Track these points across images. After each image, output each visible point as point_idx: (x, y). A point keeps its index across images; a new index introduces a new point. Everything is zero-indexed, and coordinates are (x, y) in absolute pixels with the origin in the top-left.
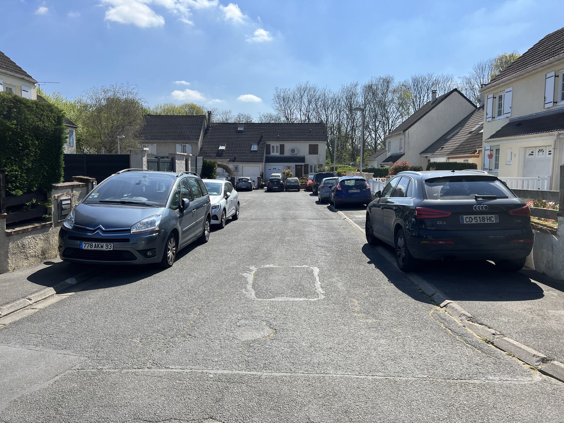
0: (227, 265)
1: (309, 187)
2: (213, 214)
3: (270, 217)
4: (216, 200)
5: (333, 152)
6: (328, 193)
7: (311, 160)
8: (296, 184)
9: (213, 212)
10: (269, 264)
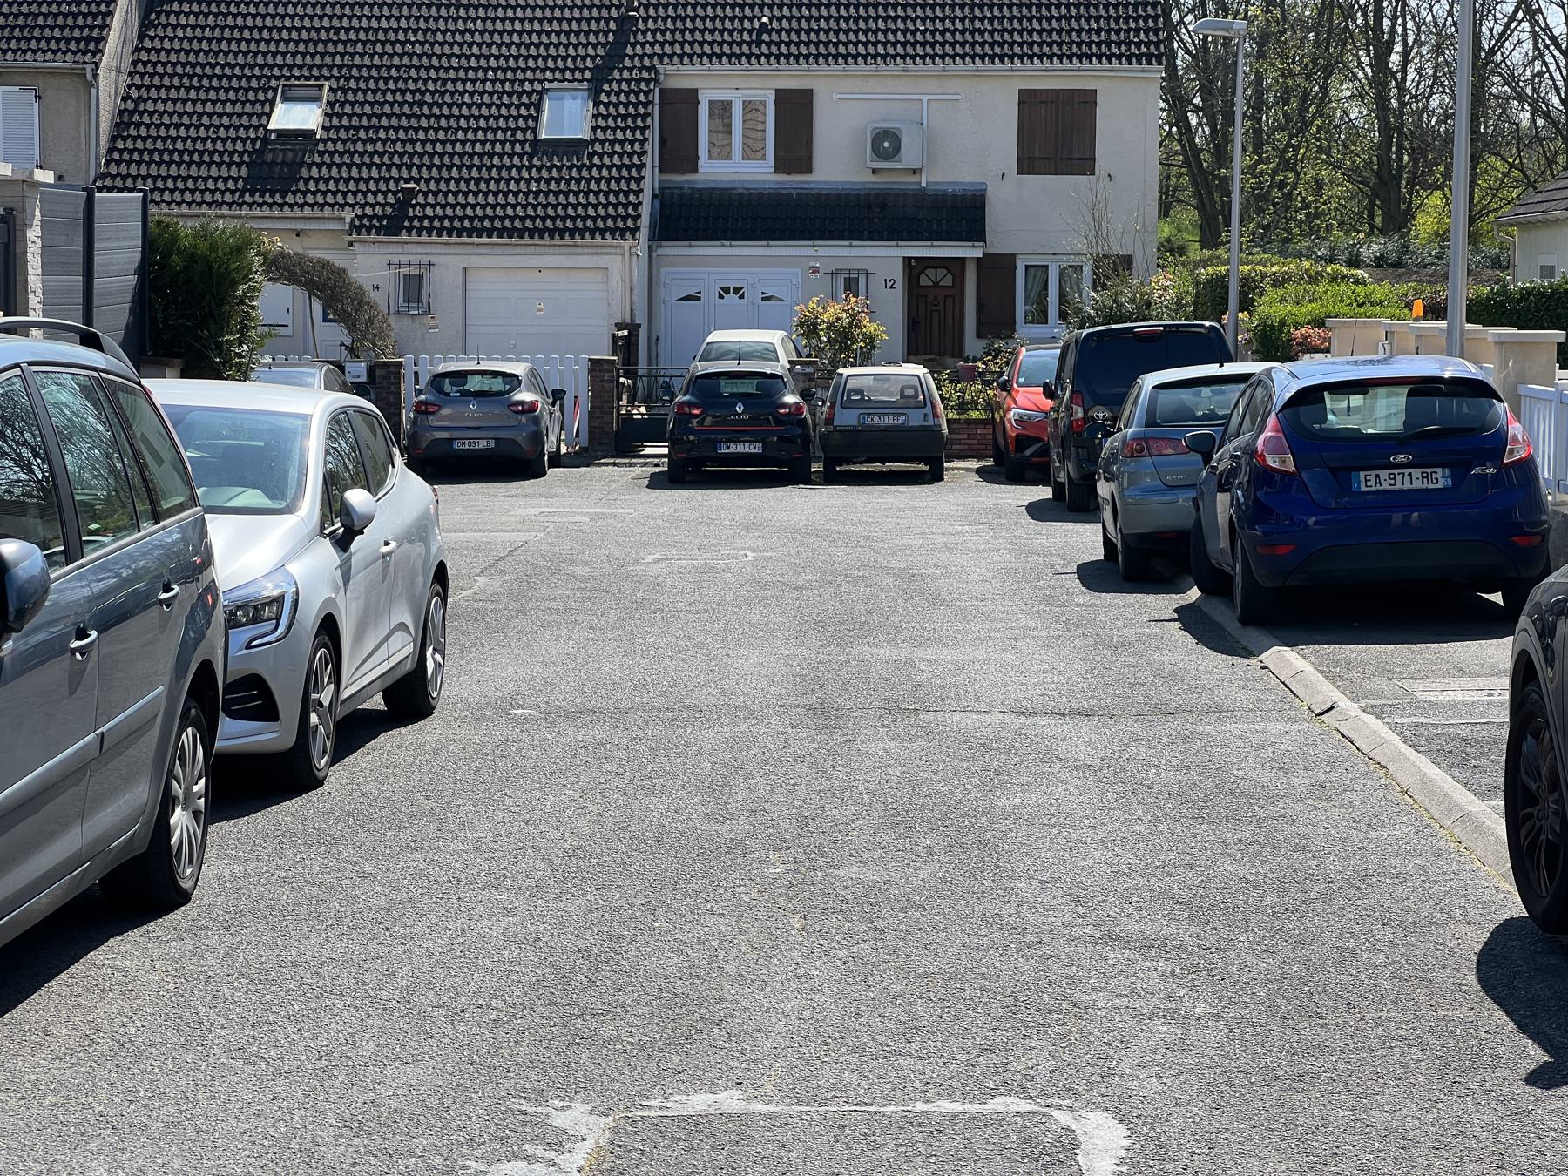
0: (359, 1098)
1: (1022, 442)
2: (238, 670)
3: (699, 698)
4: (258, 550)
5: (1222, 155)
6: (1184, 499)
7: (1037, 220)
8: (916, 419)
9: (232, 653)
10: (712, 1086)
